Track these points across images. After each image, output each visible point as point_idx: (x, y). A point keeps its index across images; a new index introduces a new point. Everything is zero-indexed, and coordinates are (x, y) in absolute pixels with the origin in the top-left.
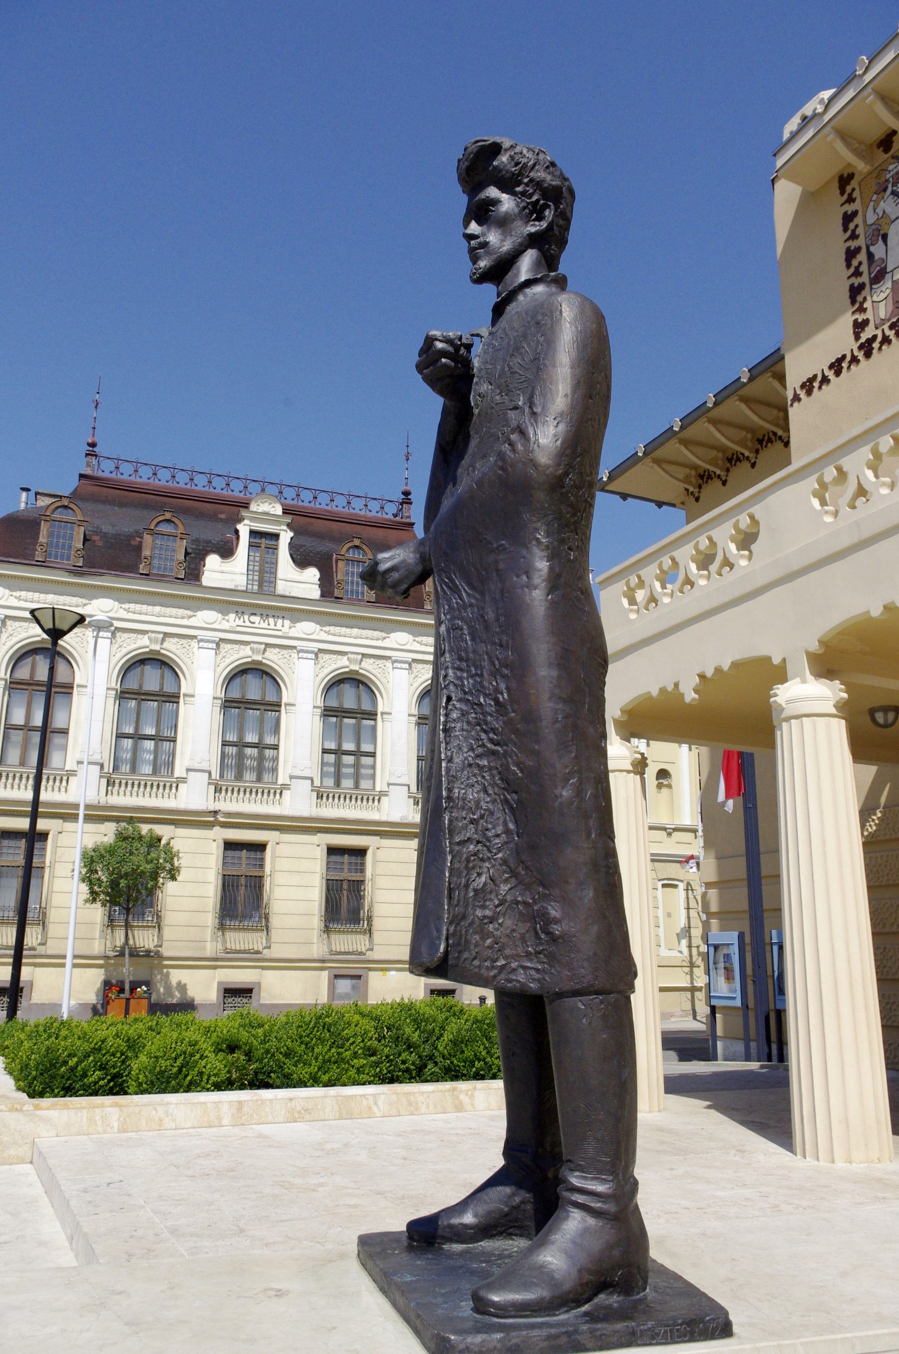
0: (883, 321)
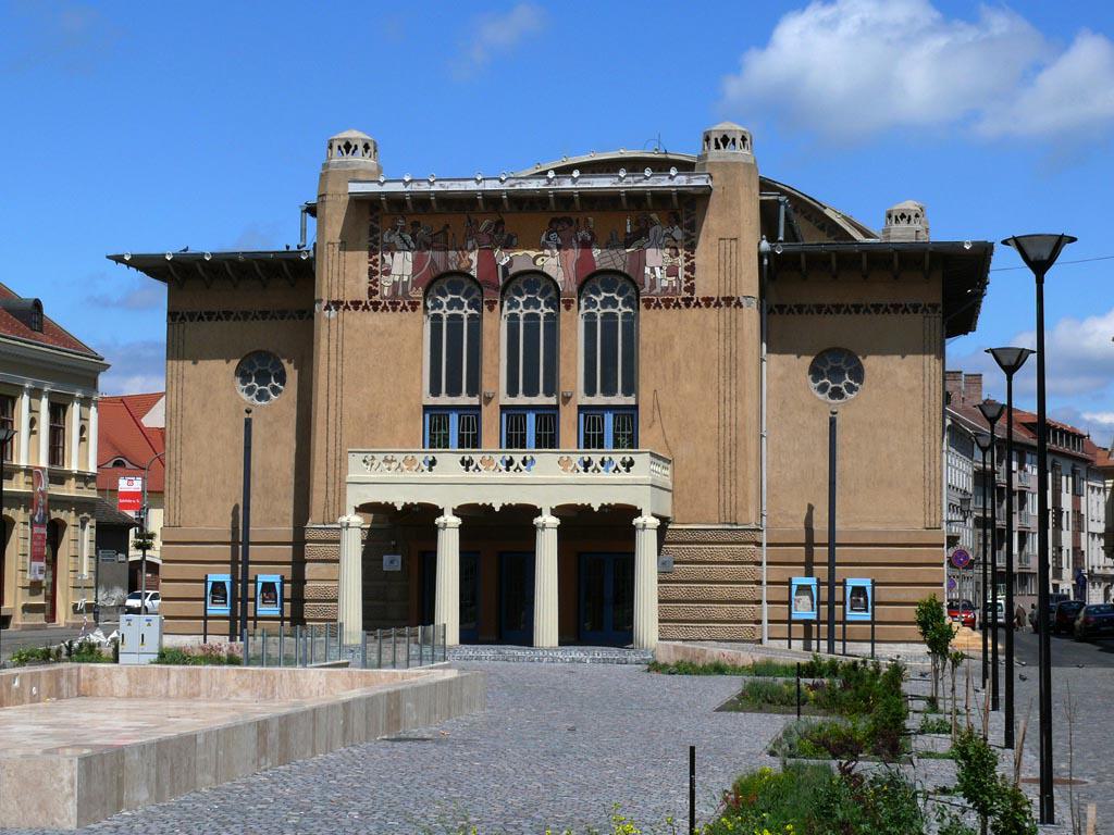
0: (385, 298)
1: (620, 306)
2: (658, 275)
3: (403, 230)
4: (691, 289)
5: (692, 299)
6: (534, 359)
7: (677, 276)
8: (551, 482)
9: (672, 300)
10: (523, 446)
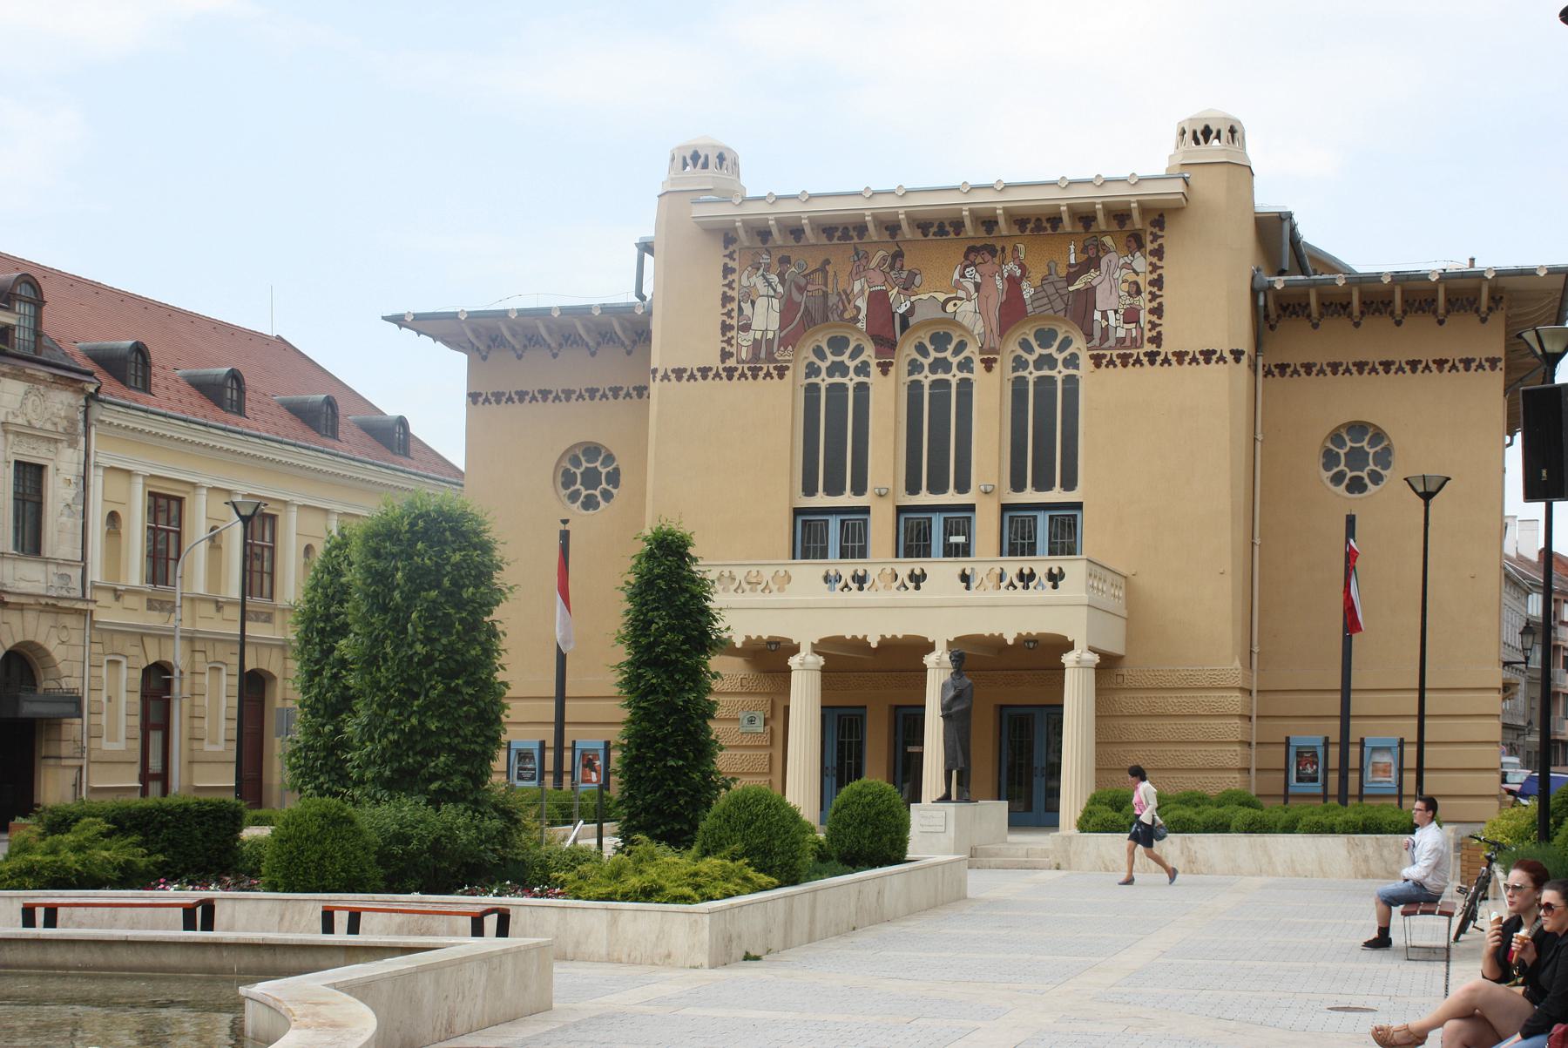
1: (1060, 366)
2: (1112, 322)
3: (767, 269)
4: (1157, 340)
5: (1158, 353)
6: (936, 447)
7: (1138, 322)
8: (950, 607)
9: (1131, 355)
10: (825, 556)
